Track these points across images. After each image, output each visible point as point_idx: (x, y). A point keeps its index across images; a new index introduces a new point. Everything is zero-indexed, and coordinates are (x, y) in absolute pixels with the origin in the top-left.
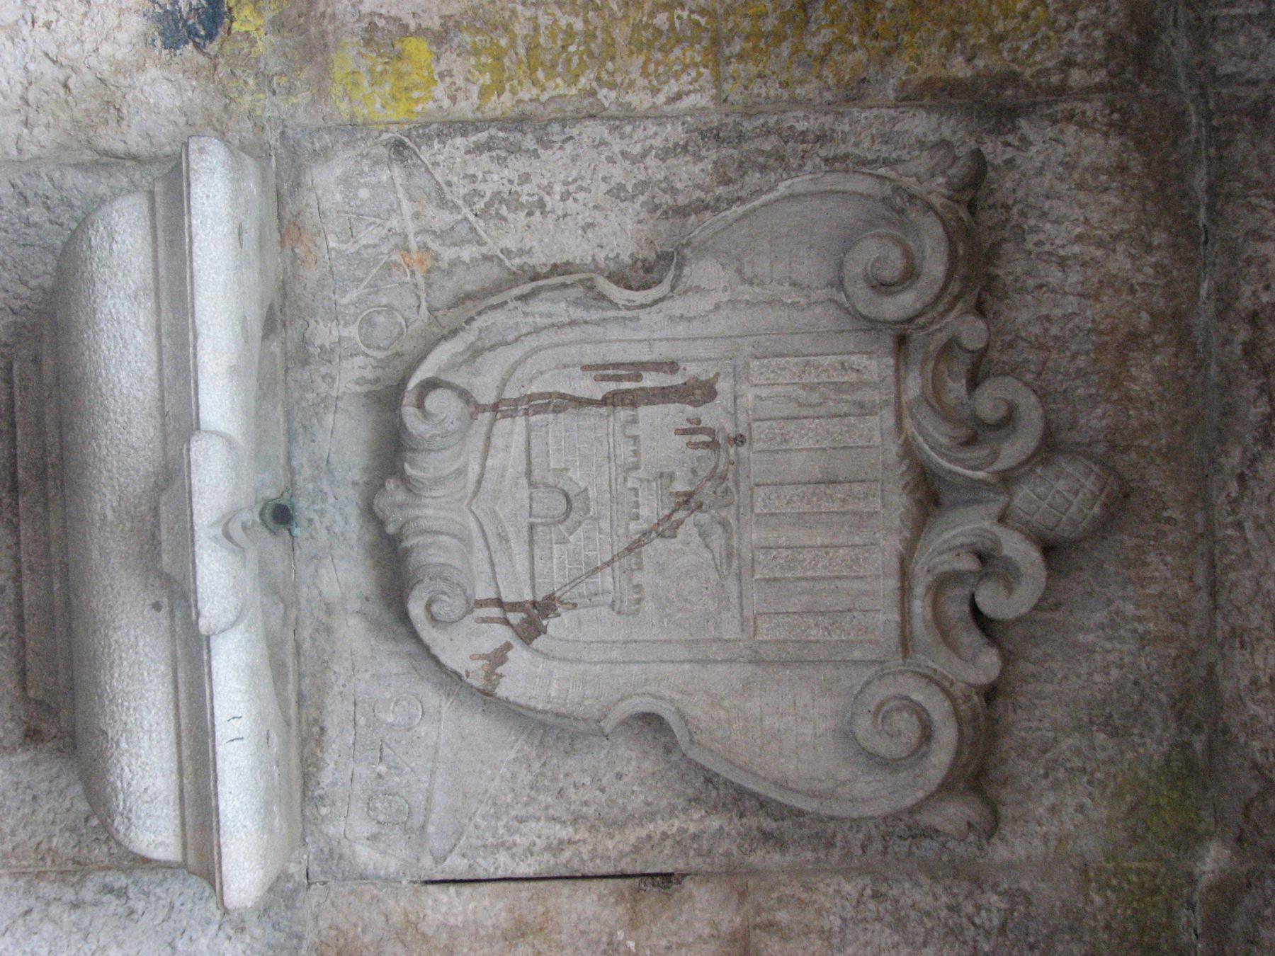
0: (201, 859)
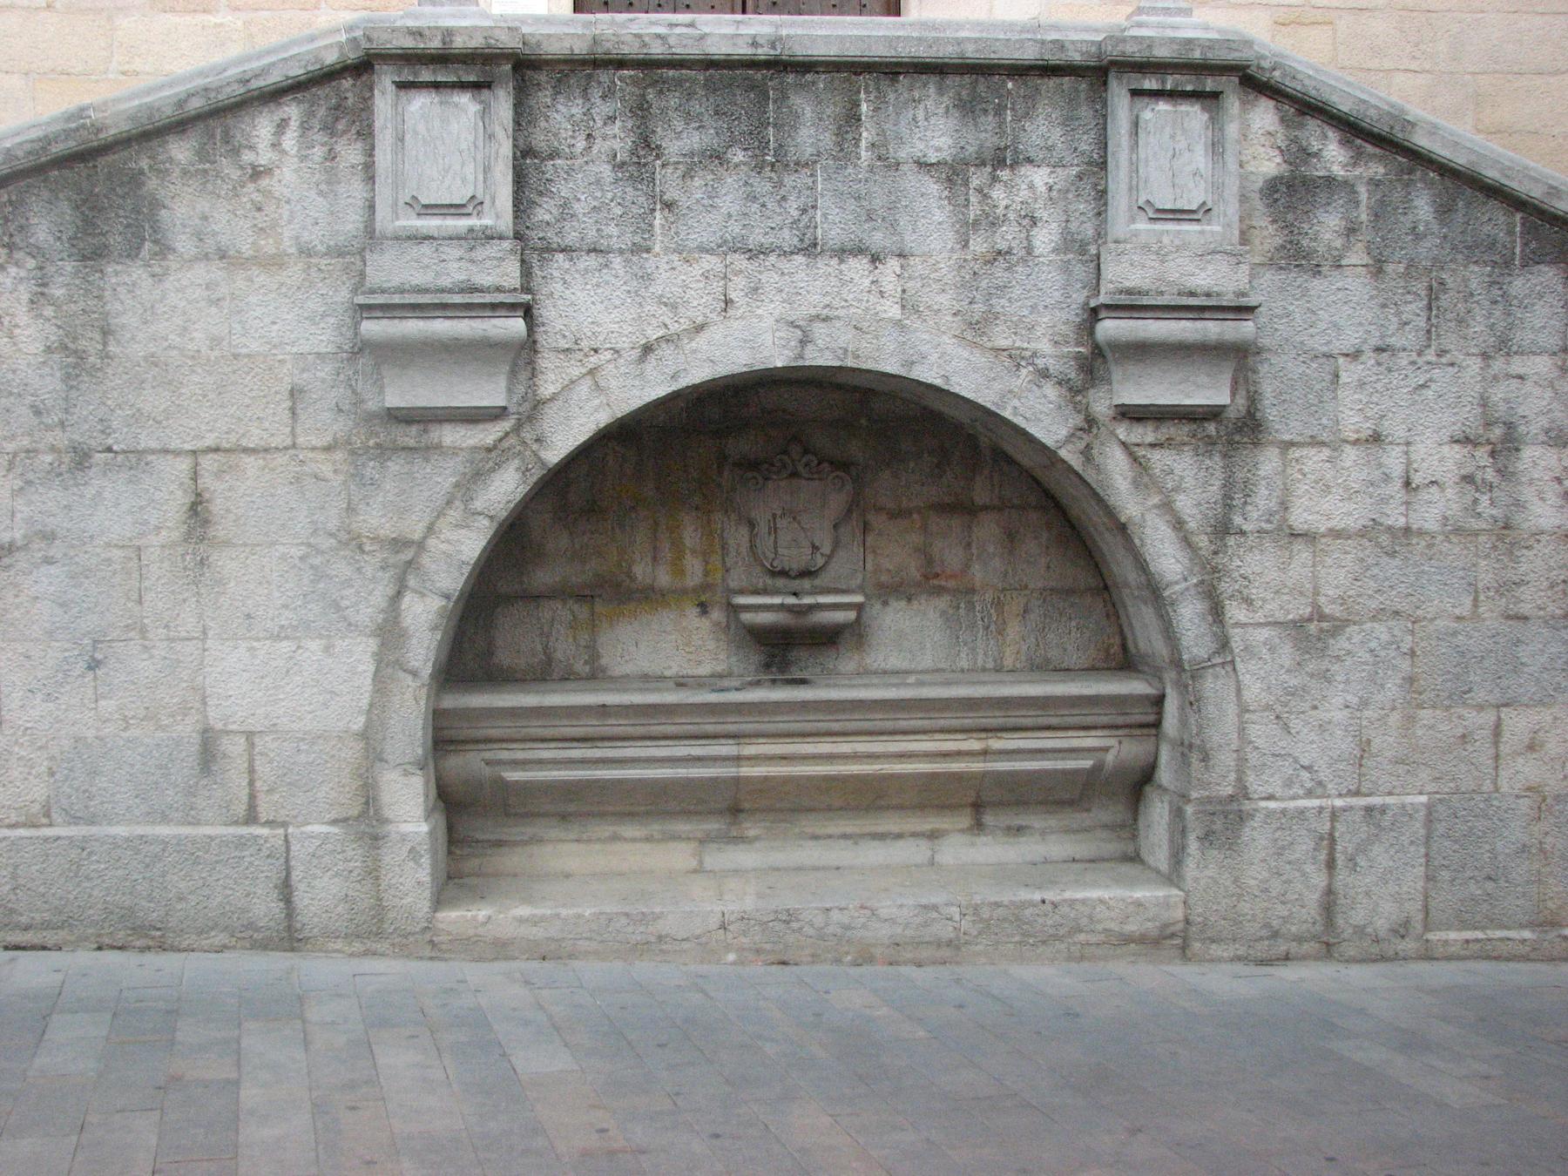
0: (859, 607)
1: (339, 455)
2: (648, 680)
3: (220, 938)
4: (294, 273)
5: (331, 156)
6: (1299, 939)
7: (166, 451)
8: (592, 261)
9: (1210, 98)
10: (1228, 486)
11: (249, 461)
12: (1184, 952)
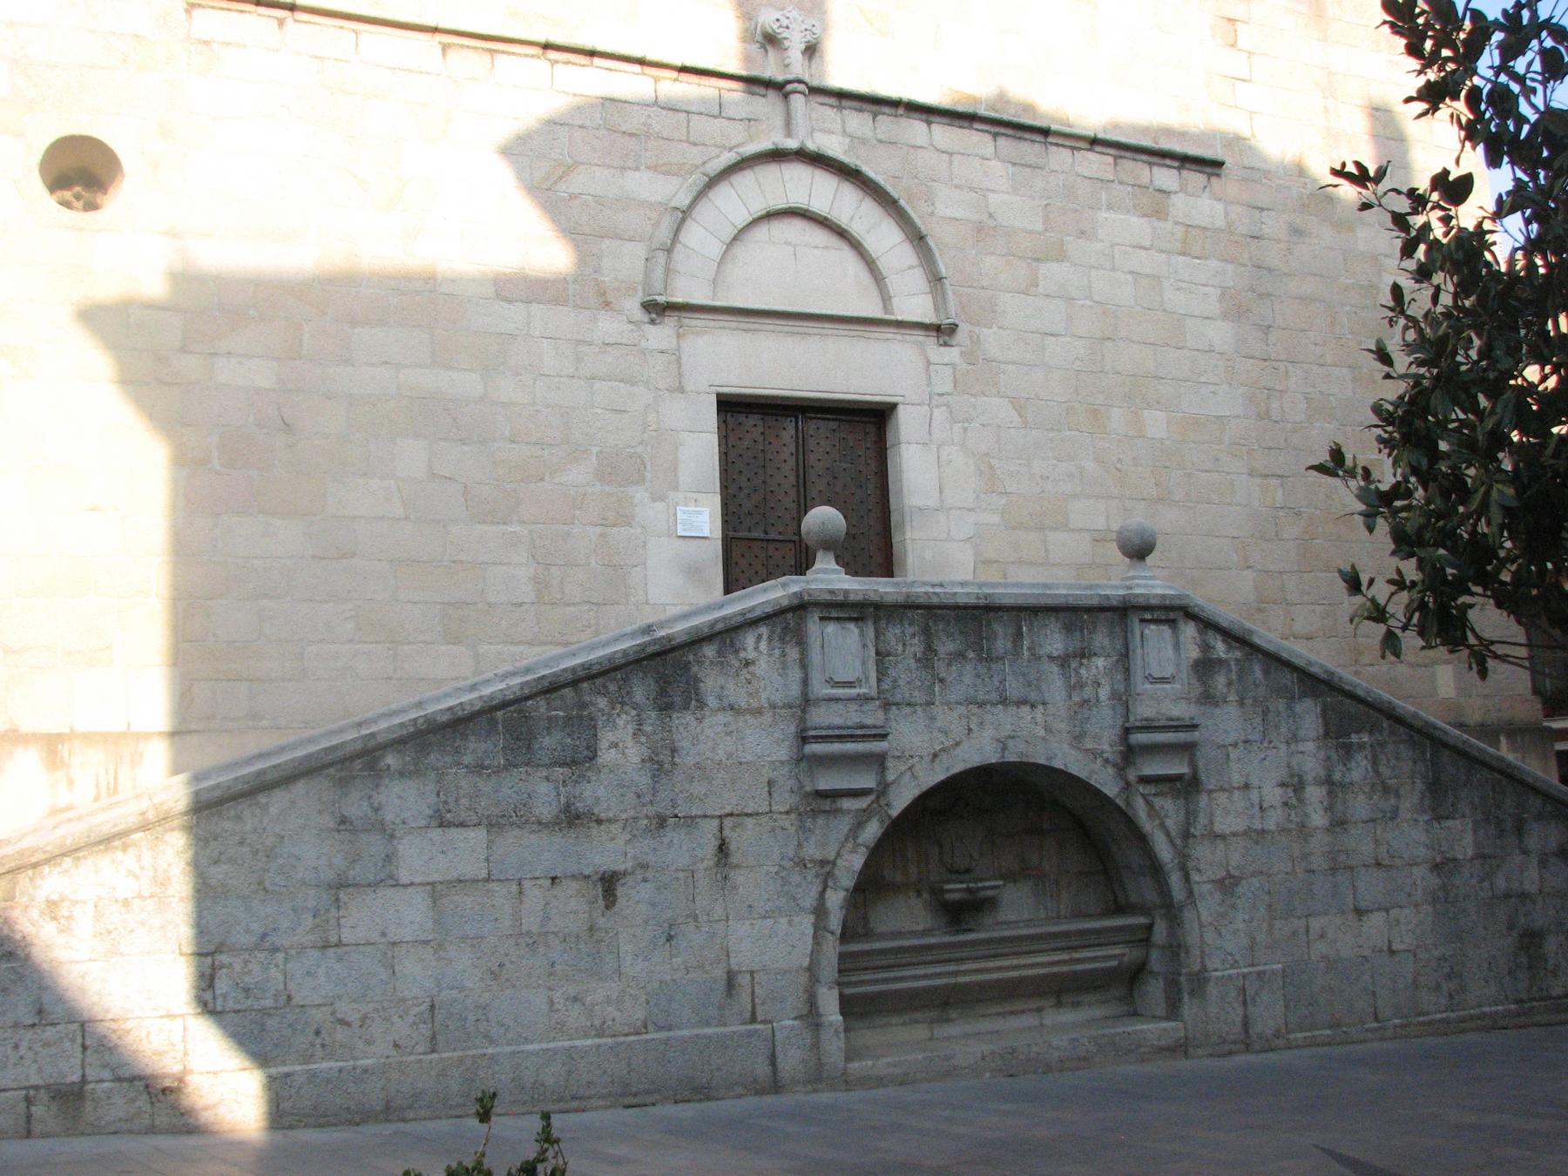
1: (793, 816)
2: (1015, 924)
3: (740, 1090)
4: (768, 718)
5: (784, 654)
6: (1234, 1042)
7: (705, 816)
8: (907, 710)
9: (1172, 623)
10: (1187, 812)
11: (749, 822)
12: (1186, 1054)
